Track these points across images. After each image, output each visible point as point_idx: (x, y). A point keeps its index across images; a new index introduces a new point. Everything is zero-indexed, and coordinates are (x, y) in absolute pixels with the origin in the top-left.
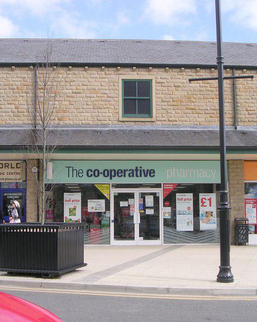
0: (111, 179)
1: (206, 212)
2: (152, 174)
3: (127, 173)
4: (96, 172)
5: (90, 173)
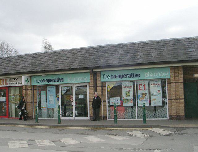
0: (121, 79)
1: (142, 94)
2: (139, 76)
3: (128, 76)
4: (115, 76)
5: (112, 77)
